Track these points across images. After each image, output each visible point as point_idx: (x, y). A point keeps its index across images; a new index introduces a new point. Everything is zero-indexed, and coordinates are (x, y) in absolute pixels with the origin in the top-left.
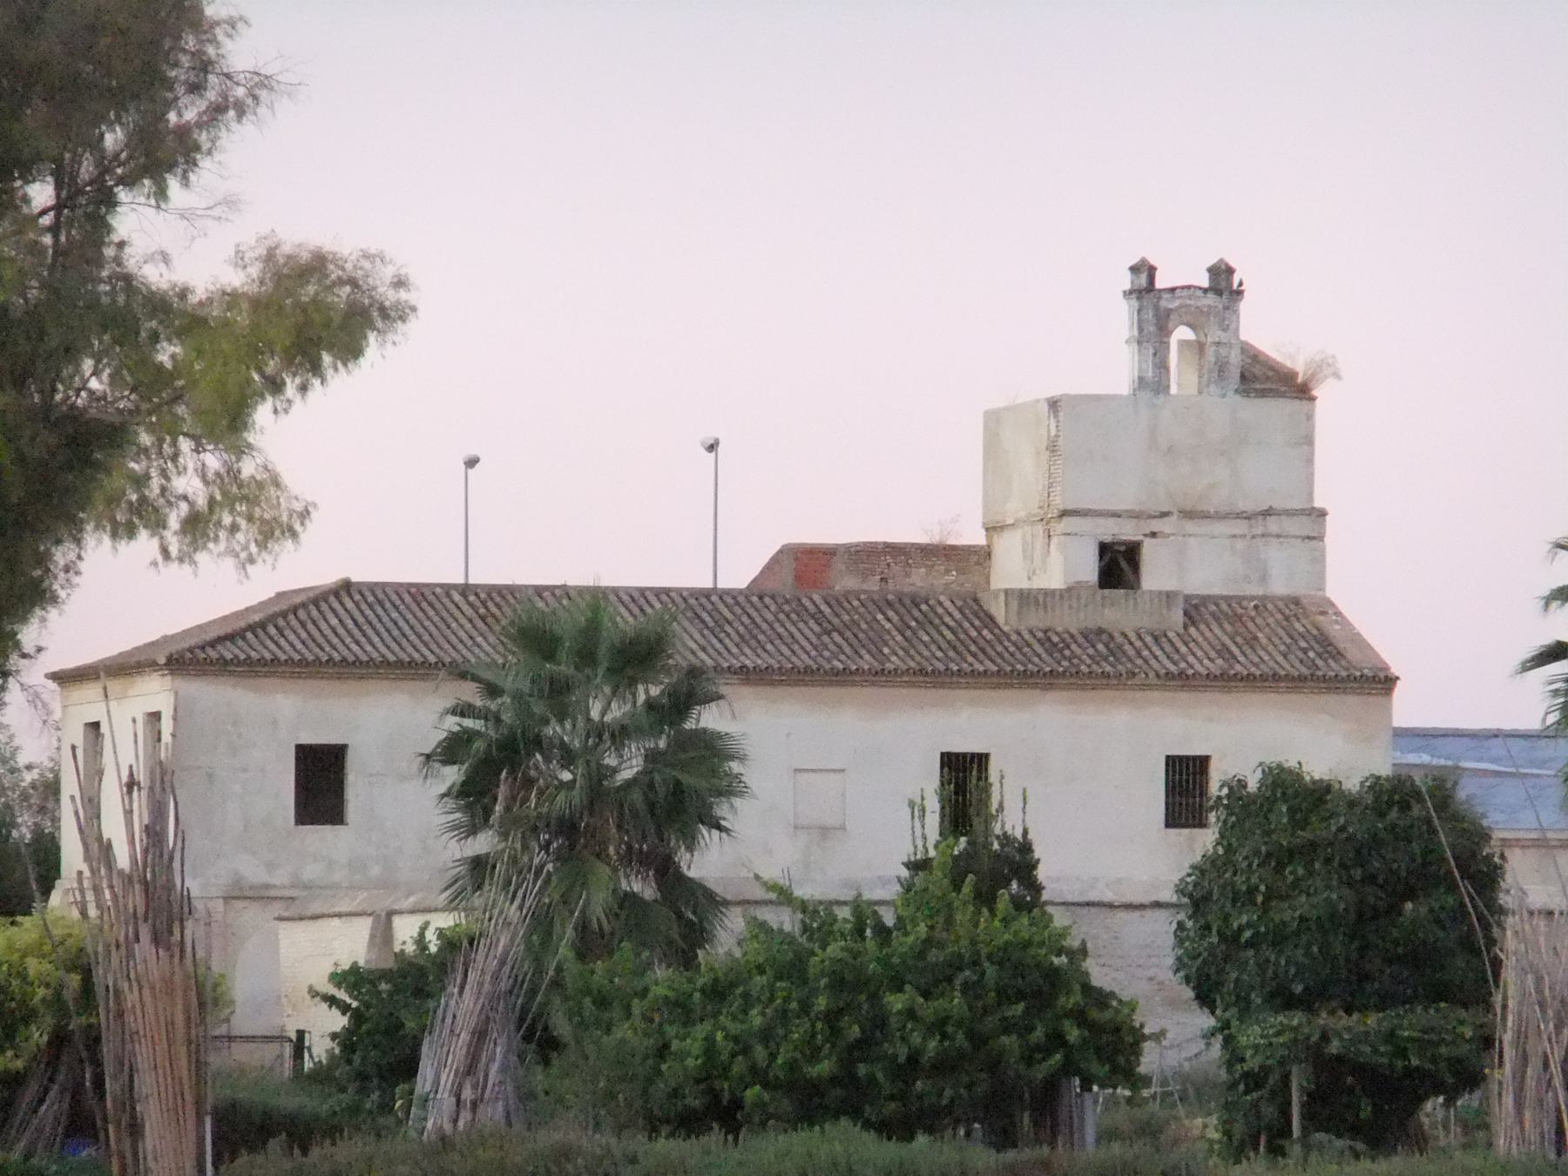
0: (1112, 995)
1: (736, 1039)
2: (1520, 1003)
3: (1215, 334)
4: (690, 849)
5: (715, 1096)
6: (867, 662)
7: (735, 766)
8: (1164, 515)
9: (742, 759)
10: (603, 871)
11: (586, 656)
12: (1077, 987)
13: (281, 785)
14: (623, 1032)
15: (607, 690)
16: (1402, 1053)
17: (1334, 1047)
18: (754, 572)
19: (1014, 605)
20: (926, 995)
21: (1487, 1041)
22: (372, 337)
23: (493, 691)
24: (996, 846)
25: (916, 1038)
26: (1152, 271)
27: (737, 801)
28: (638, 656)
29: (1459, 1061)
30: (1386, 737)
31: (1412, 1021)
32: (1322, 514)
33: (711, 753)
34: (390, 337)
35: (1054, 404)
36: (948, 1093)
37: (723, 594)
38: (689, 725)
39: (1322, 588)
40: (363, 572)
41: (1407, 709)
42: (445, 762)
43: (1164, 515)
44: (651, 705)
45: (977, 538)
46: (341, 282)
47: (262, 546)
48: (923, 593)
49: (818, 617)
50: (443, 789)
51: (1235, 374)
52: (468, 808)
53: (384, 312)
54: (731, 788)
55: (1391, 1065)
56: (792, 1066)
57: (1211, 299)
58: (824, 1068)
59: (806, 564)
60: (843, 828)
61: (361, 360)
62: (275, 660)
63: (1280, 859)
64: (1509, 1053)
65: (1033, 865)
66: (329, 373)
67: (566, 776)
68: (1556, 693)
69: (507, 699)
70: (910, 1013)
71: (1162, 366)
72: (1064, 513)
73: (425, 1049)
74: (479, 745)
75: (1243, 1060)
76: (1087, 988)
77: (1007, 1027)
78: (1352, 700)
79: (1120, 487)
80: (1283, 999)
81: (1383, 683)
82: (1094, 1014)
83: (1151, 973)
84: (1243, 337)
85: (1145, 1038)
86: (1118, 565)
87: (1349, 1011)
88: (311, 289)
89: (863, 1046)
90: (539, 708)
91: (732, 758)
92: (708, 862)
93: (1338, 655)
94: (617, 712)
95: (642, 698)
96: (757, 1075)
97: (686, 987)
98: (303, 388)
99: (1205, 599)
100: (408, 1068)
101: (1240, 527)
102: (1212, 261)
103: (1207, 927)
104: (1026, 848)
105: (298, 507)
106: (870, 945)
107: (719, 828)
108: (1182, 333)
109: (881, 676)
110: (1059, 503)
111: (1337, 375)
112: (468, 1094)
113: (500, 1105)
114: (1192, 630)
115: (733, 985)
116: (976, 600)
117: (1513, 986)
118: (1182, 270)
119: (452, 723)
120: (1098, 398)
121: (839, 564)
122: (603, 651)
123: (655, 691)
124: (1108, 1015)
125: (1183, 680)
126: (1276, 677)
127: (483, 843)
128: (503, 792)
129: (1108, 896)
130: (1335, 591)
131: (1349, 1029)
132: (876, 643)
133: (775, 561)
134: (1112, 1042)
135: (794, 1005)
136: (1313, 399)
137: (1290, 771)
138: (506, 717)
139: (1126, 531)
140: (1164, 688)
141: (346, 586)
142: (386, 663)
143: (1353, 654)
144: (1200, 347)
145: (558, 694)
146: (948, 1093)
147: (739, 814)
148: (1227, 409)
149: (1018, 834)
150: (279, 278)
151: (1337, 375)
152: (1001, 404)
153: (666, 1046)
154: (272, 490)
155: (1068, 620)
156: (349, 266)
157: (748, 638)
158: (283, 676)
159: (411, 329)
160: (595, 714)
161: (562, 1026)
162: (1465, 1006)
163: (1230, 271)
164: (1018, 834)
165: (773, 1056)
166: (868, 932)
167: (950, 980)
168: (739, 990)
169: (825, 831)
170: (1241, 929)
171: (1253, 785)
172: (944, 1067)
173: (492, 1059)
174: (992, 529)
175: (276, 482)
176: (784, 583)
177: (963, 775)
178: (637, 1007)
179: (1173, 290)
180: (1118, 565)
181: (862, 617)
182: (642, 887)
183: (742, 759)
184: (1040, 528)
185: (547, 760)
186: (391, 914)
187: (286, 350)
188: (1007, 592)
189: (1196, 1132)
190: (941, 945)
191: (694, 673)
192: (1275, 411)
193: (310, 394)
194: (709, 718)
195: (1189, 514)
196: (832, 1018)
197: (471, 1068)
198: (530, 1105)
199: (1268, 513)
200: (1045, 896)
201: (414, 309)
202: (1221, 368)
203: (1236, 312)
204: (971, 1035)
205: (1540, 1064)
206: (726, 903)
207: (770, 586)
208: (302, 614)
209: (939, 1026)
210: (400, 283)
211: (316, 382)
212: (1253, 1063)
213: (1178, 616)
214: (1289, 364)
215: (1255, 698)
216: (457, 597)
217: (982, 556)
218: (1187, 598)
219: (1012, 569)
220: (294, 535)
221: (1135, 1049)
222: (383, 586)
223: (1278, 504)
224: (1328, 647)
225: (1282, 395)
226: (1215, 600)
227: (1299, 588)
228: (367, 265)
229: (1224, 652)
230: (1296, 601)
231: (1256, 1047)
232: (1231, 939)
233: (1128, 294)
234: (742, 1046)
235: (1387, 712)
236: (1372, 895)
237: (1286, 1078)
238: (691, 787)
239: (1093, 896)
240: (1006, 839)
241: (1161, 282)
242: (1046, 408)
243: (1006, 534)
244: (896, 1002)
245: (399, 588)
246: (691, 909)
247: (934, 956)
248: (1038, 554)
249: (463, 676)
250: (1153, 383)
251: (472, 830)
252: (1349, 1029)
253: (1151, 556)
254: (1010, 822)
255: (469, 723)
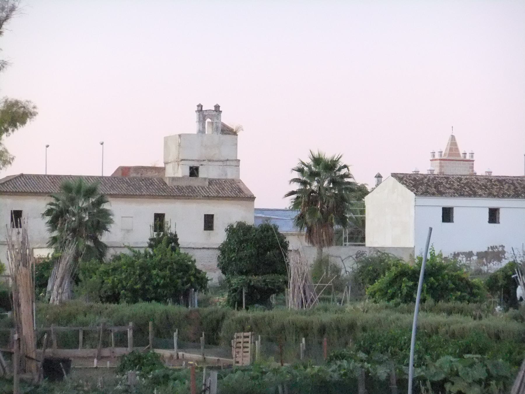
0: (201, 271)
1: (119, 280)
2: (294, 274)
3: (216, 121)
4: (101, 235)
5: (114, 293)
6: (138, 193)
7: (111, 217)
8: (204, 160)
9: (113, 215)
10: (82, 240)
11: (78, 191)
12: (194, 269)
13: (7, 219)
14: (94, 277)
15: (83, 200)
16: (267, 285)
17: (252, 284)
18: (113, 172)
19: (171, 180)
20: (160, 270)
21: (286, 283)
22: (28, 119)
23: (57, 200)
24: (169, 235)
25: (158, 280)
26: (202, 106)
27: (112, 225)
28: (90, 192)
29: (279, 286)
30: (253, 211)
31: (269, 278)
32: (239, 161)
33: (106, 214)
34: (32, 119)
35: (180, 136)
36: (165, 292)
37: (106, 177)
38: (101, 207)
39: (239, 177)
40: (25, 172)
41: (258, 204)
42: (47, 216)
43: (204, 160)
44: (93, 204)
45: (162, 165)
46: (21, 107)
47: (4, 166)
48: (150, 177)
49: (127, 182)
50: (47, 221)
51: (220, 129)
52: (52, 226)
53: (31, 114)
54: (111, 222)
55: (264, 287)
56: (132, 286)
57: (215, 113)
58: (138, 286)
59: (124, 171)
60: (132, 230)
61: (26, 125)
62: (6, 192)
63: (241, 242)
64: (291, 285)
65: (178, 239)
66: (19, 127)
67: (74, 219)
68: (292, 202)
69: (60, 202)
70: (157, 275)
71: (204, 128)
72: (182, 160)
73: (49, 281)
74: (54, 212)
75: (232, 286)
76: (196, 269)
77: (178, 278)
78: (244, 202)
79: (194, 154)
80: (241, 273)
81: (252, 198)
82: (198, 275)
83: (203, 263)
84: (222, 121)
85: (208, 280)
86: (194, 172)
87: (255, 275)
88: (15, 109)
89: (147, 282)
90: (68, 203)
91: (110, 215)
92: (105, 238)
93: (242, 192)
94: (85, 205)
95: (91, 202)
96: (123, 288)
97: (108, 268)
98: (13, 131)
99: (213, 179)
100: (46, 285)
101: (221, 163)
102: (215, 104)
103: (225, 257)
104: (176, 236)
105: (12, 157)
106: (148, 259)
107: (107, 230)
108: (208, 120)
109: (141, 196)
110: (181, 157)
111: (242, 130)
112: (60, 291)
113: (67, 294)
114: (210, 187)
115: (118, 268)
116: (162, 179)
117: (293, 271)
118: (209, 106)
119: (49, 207)
120: (188, 134)
121: (131, 171)
122: (82, 191)
123: (93, 200)
124: (201, 275)
125: (209, 198)
126: (229, 197)
127: (55, 234)
128: (60, 222)
129: (193, 246)
130: (241, 178)
131: (256, 279)
132: (140, 188)
133: (117, 170)
134: (200, 281)
135: (132, 273)
136: (237, 135)
137: (243, 223)
138: (60, 205)
139: (195, 164)
140: (203, 199)
141: (22, 175)
142: (31, 192)
143: (246, 192)
144: (212, 123)
145: (72, 201)
146: (165, 292)
147: (112, 227)
148: (218, 137)
149: (174, 233)
150: (8, 106)
151: (242, 130)
152: (168, 135)
153: (103, 281)
154: (6, 153)
155: (183, 184)
156: (23, 104)
157: (112, 187)
158: (8, 195)
159: (37, 118)
160: (80, 205)
161: (81, 277)
162: (281, 274)
163: (219, 107)
164: (174, 233)
165: (127, 284)
166: (148, 256)
167: (166, 267)
168: (120, 269)
169: (128, 231)
170: (232, 257)
171: (235, 227)
172: (165, 286)
173: (65, 283)
174: (166, 163)
175: (7, 151)
176: (120, 175)
177: (159, 218)
178: (97, 272)
179: (206, 111)
180: (194, 172)
181: (137, 183)
182: (90, 243)
183: (113, 215)
184: (176, 163)
185: (70, 215)
186: (33, 249)
187: (9, 122)
188: (169, 177)
189: (217, 300)
190: (164, 259)
191: (102, 196)
192: (229, 137)
193: (15, 132)
194: (105, 206)
195: (209, 161)
196: (140, 275)
197: (60, 286)
198: (73, 295)
199: (227, 160)
200: (180, 246)
201: (37, 113)
202: (217, 128)
203: (220, 116)
204: (170, 279)
205: (298, 288)
206: (109, 247)
207: (116, 176)
208: (12, 181)
209: (164, 278)
210: (34, 107)
211: (16, 129)
212: (235, 287)
213: (207, 183)
214: (232, 127)
215: (225, 201)
216: (47, 178)
217: (162, 170)
218: (209, 179)
219: (170, 173)
220: (10, 163)
221: (206, 282)
222: (31, 175)
223: (229, 158)
224: (240, 190)
225: (229, 134)
226: (215, 180)
227: (233, 177)
228: (27, 103)
229: (217, 191)
230: (233, 180)
231: (235, 283)
232: (230, 260)
233: (196, 111)
234: (120, 281)
235: (253, 205)
236: (261, 251)
237: (242, 289)
238: (100, 221)
239: (189, 246)
240: (171, 234)
241: (203, 109)
242: (178, 136)
243: (169, 164)
244: (154, 272)
245: (34, 176)
246: (100, 249)
247: (162, 262)
248: (176, 169)
249: (51, 196)
250: (202, 131)
251: (53, 231)
252: (256, 279)
253: (201, 170)
254: (173, 230)
255: (52, 207)
